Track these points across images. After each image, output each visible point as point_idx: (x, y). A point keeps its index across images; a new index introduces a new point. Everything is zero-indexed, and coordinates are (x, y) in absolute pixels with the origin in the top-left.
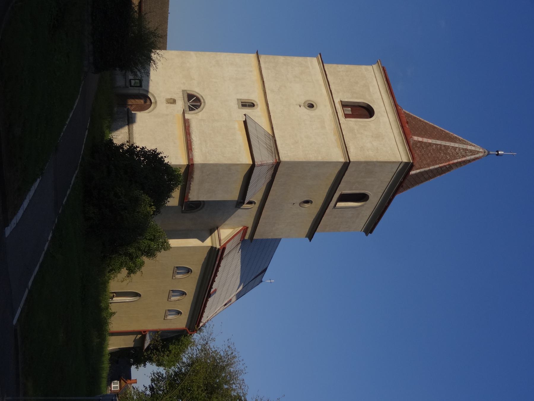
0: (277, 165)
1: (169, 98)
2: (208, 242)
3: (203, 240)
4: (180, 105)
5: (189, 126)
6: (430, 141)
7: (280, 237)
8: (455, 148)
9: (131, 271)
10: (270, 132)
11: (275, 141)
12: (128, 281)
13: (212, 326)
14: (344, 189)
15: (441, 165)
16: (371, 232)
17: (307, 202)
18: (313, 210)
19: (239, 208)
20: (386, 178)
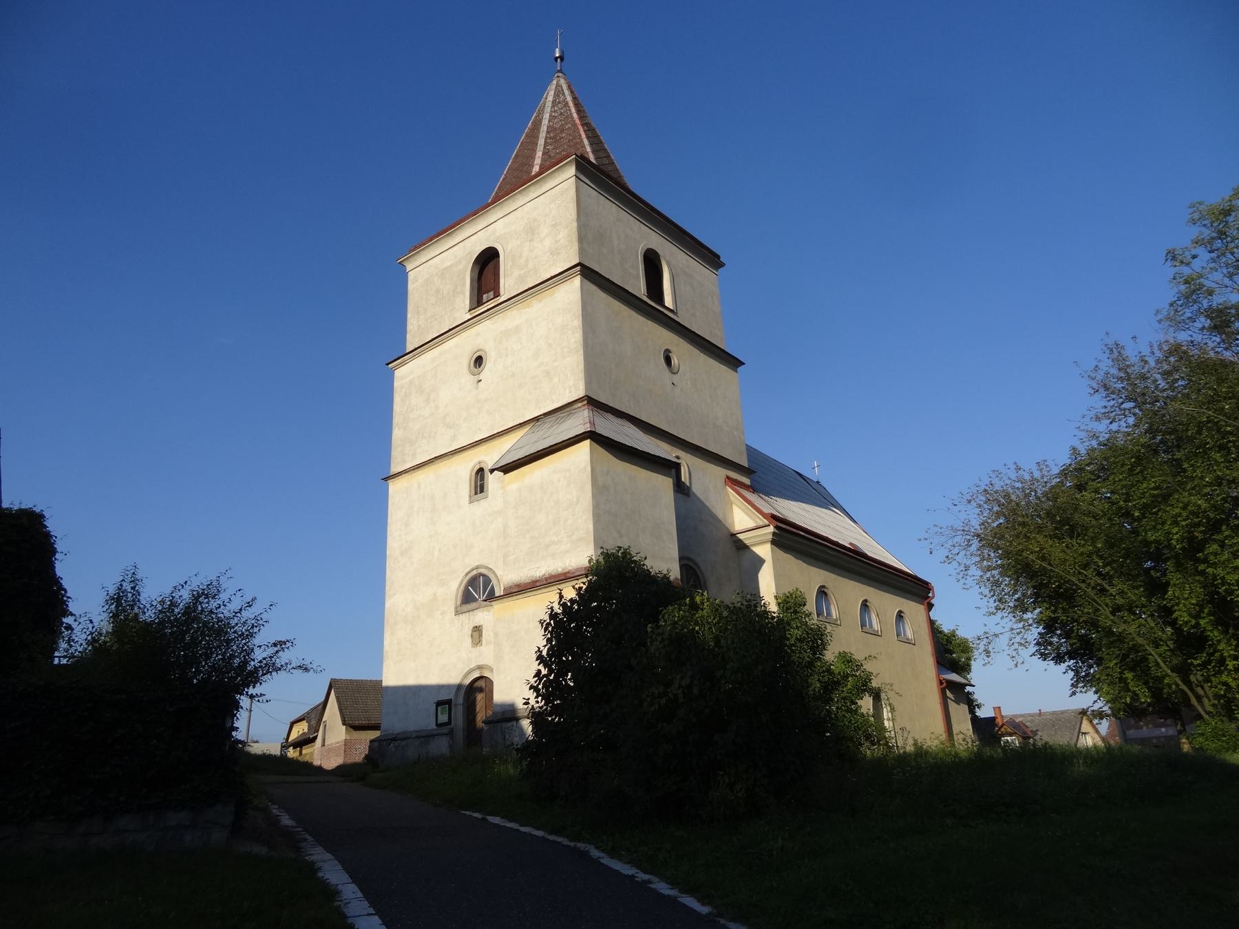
0: (591, 402)
1: (470, 640)
2: (764, 551)
3: (761, 561)
4: (485, 616)
5: (518, 586)
6: (539, 154)
7: (744, 448)
8: (552, 118)
9: (864, 686)
10: (526, 429)
11: (546, 415)
12: (891, 694)
13: (937, 529)
14: (639, 288)
15: (583, 136)
16: (718, 257)
17: (668, 360)
18: (682, 351)
19: (689, 489)
20: (609, 211)
